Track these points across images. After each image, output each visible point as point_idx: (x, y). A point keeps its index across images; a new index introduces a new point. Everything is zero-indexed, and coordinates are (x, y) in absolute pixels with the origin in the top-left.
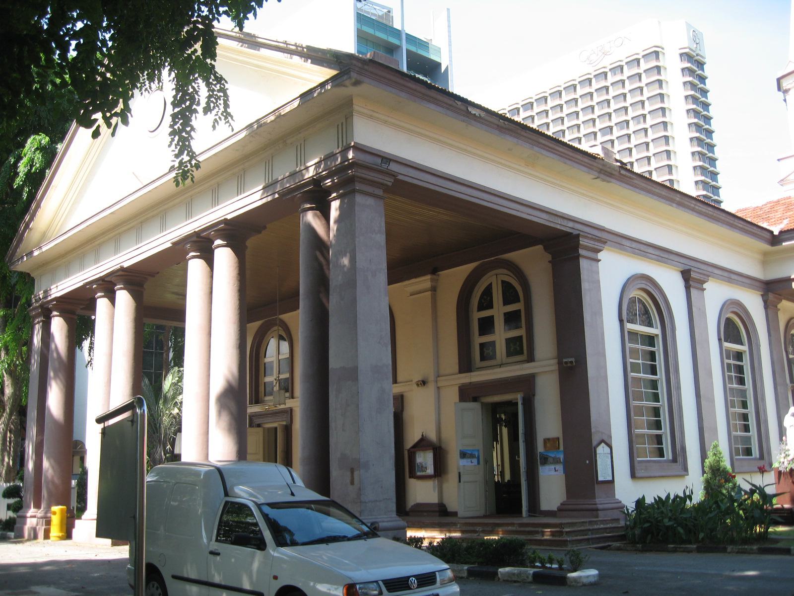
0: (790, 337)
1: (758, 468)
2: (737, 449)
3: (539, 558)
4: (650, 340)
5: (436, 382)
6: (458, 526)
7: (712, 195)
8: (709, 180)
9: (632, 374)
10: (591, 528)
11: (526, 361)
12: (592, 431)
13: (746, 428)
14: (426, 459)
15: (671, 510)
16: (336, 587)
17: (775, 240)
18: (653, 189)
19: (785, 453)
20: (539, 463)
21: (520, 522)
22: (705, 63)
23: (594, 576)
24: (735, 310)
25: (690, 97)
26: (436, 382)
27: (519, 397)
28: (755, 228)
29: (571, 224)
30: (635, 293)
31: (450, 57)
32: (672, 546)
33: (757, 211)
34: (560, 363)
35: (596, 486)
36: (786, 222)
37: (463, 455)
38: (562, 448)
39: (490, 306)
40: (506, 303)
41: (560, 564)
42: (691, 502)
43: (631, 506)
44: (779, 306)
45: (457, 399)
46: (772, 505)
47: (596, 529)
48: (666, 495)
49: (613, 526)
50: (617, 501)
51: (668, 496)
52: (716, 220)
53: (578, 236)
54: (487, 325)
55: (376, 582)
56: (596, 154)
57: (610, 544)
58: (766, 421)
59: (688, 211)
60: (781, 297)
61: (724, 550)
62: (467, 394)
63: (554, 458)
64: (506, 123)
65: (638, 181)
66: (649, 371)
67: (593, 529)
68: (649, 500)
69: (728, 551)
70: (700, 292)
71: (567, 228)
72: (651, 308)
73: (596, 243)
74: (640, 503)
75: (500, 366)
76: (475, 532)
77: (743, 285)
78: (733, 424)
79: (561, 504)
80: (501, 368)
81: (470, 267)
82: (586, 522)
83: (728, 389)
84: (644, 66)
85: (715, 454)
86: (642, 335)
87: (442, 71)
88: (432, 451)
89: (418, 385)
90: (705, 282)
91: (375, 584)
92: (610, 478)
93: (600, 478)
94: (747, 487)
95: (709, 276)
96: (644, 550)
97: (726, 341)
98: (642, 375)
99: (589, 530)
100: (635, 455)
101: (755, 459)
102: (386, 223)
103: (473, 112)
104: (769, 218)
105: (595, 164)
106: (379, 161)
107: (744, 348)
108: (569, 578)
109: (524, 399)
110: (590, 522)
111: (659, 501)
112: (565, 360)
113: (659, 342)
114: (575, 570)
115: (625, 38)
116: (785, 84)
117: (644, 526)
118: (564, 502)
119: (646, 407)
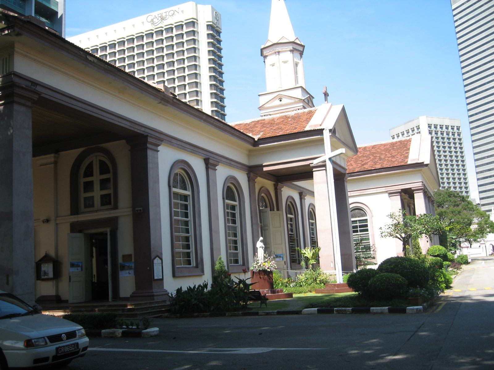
0: (261, 197)
1: (243, 270)
2: (231, 260)
3: (125, 323)
4: (185, 198)
5: (56, 220)
6: (70, 309)
7: (220, 111)
8: (219, 102)
9: (175, 217)
10: (150, 306)
11: (112, 208)
12: (151, 250)
13: (236, 248)
14: (48, 268)
15: (196, 294)
16: (15, 341)
17: (255, 143)
18: (191, 111)
19: (256, 262)
20: (119, 269)
21: (108, 304)
22: (221, 32)
23: (156, 331)
24: (232, 182)
25: (211, 51)
26: (56, 220)
27: (108, 230)
28: (245, 136)
29: (143, 129)
30: (178, 171)
31: (65, 9)
32: (196, 314)
33: (246, 126)
34: (134, 210)
35: (153, 282)
36: (261, 133)
37: (72, 265)
38: (133, 260)
39: (91, 175)
40: (102, 173)
41: (137, 325)
42: (207, 289)
43: (174, 293)
44: (256, 180)
45: (69, 232)
46: (249, 289)
47: (153, 307)
48: (194, 285)
49: (163, 305)
50: (165, 290)
51: (195, 287)
52: (225, 131)
53: (147, 137)
54: (89, 186)
55: (44, 338)
56: (160, 89)
57: (162, 315)
58: (247, 244)
59: (209, 125)
60: (257, 175)
61: (224, 315)
62: (75, 228)
63: (129, 266)
64: (109, 67)
65: (183, 106)
66: (184, 216)
67: (151, 307)
68: (184, 289)
69: (226, 315)
70: (214, 171)
71: (141, 131)
72: (186, 178)
73: (157, 141)
74: (179, 291)
75: (97, 211)
76: (81, 311)
77: (236, 167)
78: (229, 246)
79: (132, 293)
80: (97, 213)
81: (80, 150)
82: (147, 303)
83: (227, 226)
84: (185, 30)
85: (220, 263)
86: (180, 195)
87: (59, 18)
88: (52, 263)
89: (43, 222)
90: (216, 166)
91: (43, 339)
92: (161, 278)
93: (156, 278)
94: (237, 281)
95: (219, 162)
96: (181, 317)
97: (227, 199)
98: (180, 218)
99: (149, 307)
100: (175, 264)
101: (240, 265)
102: (33, 122)
103: (90, 59)
104: (253, 131)
105: (159, 95)
106: (30, 84)
107: (236, 203)
108: (143, 333)
109: (111, 231)
110: (150, 303)
111: (190, 289)
112: (136, 209)
113: (190, 199)
114: (146, 329)
115: (175, 11)
116: (265, 53)
117: (181, 304)
118: (134, 292)
119: (181, 236)
